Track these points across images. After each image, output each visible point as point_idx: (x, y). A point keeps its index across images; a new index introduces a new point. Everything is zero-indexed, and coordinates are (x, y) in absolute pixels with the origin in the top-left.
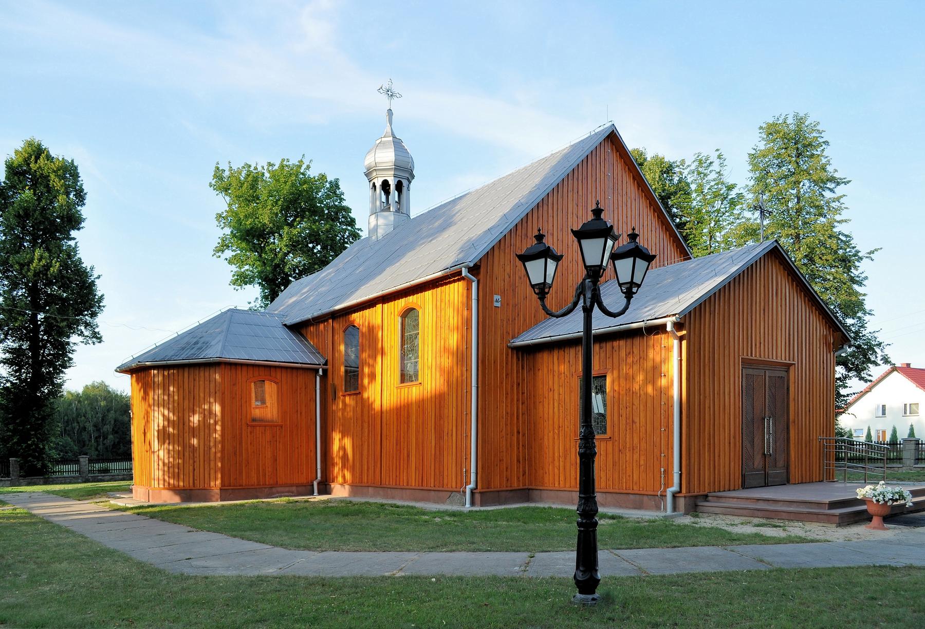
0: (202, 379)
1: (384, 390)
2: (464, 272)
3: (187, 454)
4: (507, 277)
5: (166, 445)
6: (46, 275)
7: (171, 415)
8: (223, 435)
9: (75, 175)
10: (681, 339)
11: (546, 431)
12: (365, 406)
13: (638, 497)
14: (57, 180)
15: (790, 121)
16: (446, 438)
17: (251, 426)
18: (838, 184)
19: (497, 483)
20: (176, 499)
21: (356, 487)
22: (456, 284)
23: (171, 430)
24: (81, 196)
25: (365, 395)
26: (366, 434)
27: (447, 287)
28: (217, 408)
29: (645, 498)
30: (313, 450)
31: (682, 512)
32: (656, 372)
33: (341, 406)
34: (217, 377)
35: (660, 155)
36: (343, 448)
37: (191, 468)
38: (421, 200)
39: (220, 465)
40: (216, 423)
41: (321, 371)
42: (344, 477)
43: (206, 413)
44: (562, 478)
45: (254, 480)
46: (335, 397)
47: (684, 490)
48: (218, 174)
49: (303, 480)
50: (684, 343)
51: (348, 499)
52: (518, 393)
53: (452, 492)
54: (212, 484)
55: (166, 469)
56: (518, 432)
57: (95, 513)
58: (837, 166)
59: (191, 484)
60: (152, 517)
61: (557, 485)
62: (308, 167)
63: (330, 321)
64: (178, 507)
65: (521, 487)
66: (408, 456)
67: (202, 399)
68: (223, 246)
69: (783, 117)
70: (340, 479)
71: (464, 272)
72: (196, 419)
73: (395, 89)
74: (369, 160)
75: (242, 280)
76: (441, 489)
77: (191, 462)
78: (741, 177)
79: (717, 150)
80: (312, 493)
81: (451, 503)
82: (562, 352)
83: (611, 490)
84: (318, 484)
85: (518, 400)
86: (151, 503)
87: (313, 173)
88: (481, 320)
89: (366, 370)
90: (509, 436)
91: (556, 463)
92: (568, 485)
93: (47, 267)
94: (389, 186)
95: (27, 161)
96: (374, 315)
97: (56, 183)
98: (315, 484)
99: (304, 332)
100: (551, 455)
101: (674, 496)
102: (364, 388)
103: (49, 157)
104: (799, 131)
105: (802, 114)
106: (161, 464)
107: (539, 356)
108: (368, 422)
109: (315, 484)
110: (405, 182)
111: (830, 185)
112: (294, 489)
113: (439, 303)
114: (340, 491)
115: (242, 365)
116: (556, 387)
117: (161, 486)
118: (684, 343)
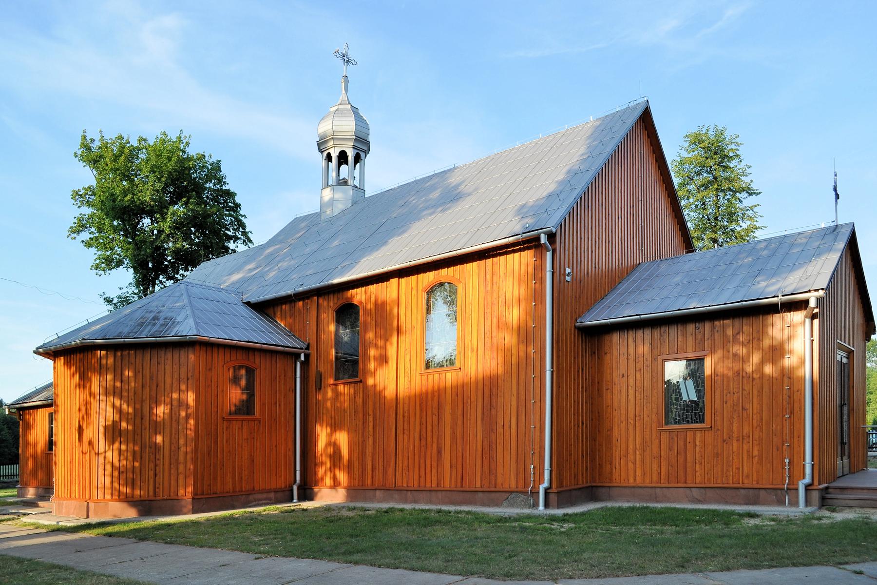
0: (169, 362)
1: (395, 375)
2: (115, 301)
3: (146, 456)
5: (116, 445)
7: (125, 406)
8: (197, 431)
11: (616, 421)
12: (374, 396)
13: (751, 491)
16: (500, 430)
17: (229, 421)
18: (750, 194)
20: (131, 513)
21: (354, 491)
22: (517, 255)
23: (124, 425)
25: (370, 382)
26: (371, 428)
27: (502, 258)
28: (191, 398)
29: (762, 493)
32: (777, 352)
33: (330, 394)
36: (335, 446)
37: (152, 473)
38: (380, 174)
39: (192, 467)
40: (188, 417)
42: (335, 479)
43: (175, 403)
44: (639, 472)
45: (229, 486)
46: (319, 387)
47: (554, 486)
48: (86, 146)
49: (281, 484)
51: (346, 505)
53: (512, 492)
54: (181, 492)
55: (116, 474)
58: (755, 178)
59: (151, 493)
60: (110, 536)
61: (631, 480)
62: (188, 144)
63: (315, 298)
66: (439, 452)
67: (168, 386)
68: (81, 226)
70: (328, 481)
71: (543, 239)
72: (161, 411)
73: (351, 55)
74: (326, 127)
75: (109, 263)
76: (493, 489)
77: (152, 465)
80: (291, 500)
81: (511, 505)
82: (622, 333)
83: (712, 485)
84: (298, 489)
86: (93, 520)
87: (192, 151)
89: (372, 352)
91: (631, 457)
92: (647, 481)
94: (347, 157)
96: (389, 290)
98: (295, 488)
99: (270, 311)
100: (623, 446)
101: (808, 488)
102: (367, 372)
105: (720, 128)
106: (108, 467)
107: (607, 338)
108: (375, 416)
109: (295, 488)
110: (362, 155)
111: (744, 195)
112: (272, 495)
113: (489, 277)
114: (329, 496)
116: (631, 371)
117: (108, 497)
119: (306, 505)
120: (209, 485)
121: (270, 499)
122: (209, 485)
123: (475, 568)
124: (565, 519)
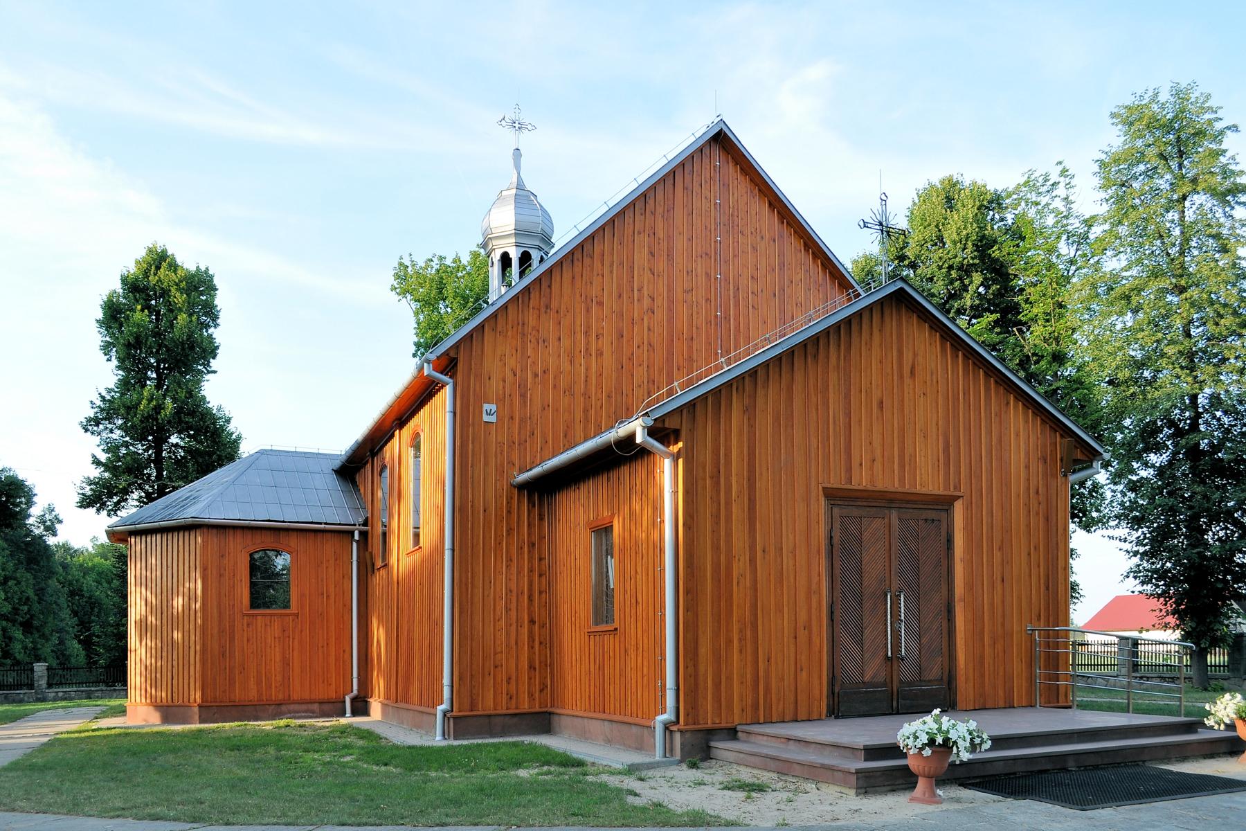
4: (509, 375)
6: (157, 419)
9: (211, 288)
10: (675, 458)
12: (1198, 624)
14: (178, 295)
15: (1164, 96)
19: (488, 703)
24: (211, 312)
30: (348, 649)
31: (678, 757)
34: (199, 540)
35: (980, 182)
41: (356, 533)
45: (253, 694)
50: (681, 461)
52: (531, 559)
56: (532, 622)
57: (68, 732)
64: (155, 729)
65: (537, 709)
69: (1150, 93)
73: (525, 118)
78: (1090, 199)
79: (1060, 163)
85: (531, 570)
88: (458, 444)
90: (513, 628)
93: (159, 408)
95: (146, 274)
97: (179, 299)
101: (667, 727)
103: (174, 266)
104: (1181, 113)
105: (1183, 85)
112: (316, 707)
115: (235, 528)
118: (681, 461)
119: (359, 720)
120: (224, 692)
121: (313, 712)
122: (224, 692)
123: (449, 820)
124: (236, 745)
